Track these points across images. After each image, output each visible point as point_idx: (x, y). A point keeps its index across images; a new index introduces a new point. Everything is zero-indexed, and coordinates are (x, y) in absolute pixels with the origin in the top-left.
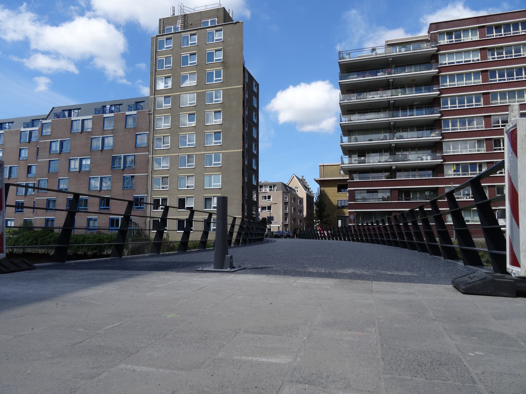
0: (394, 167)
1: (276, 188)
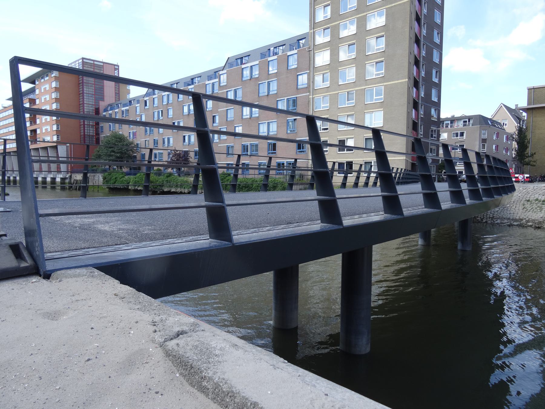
1: (471, 122)
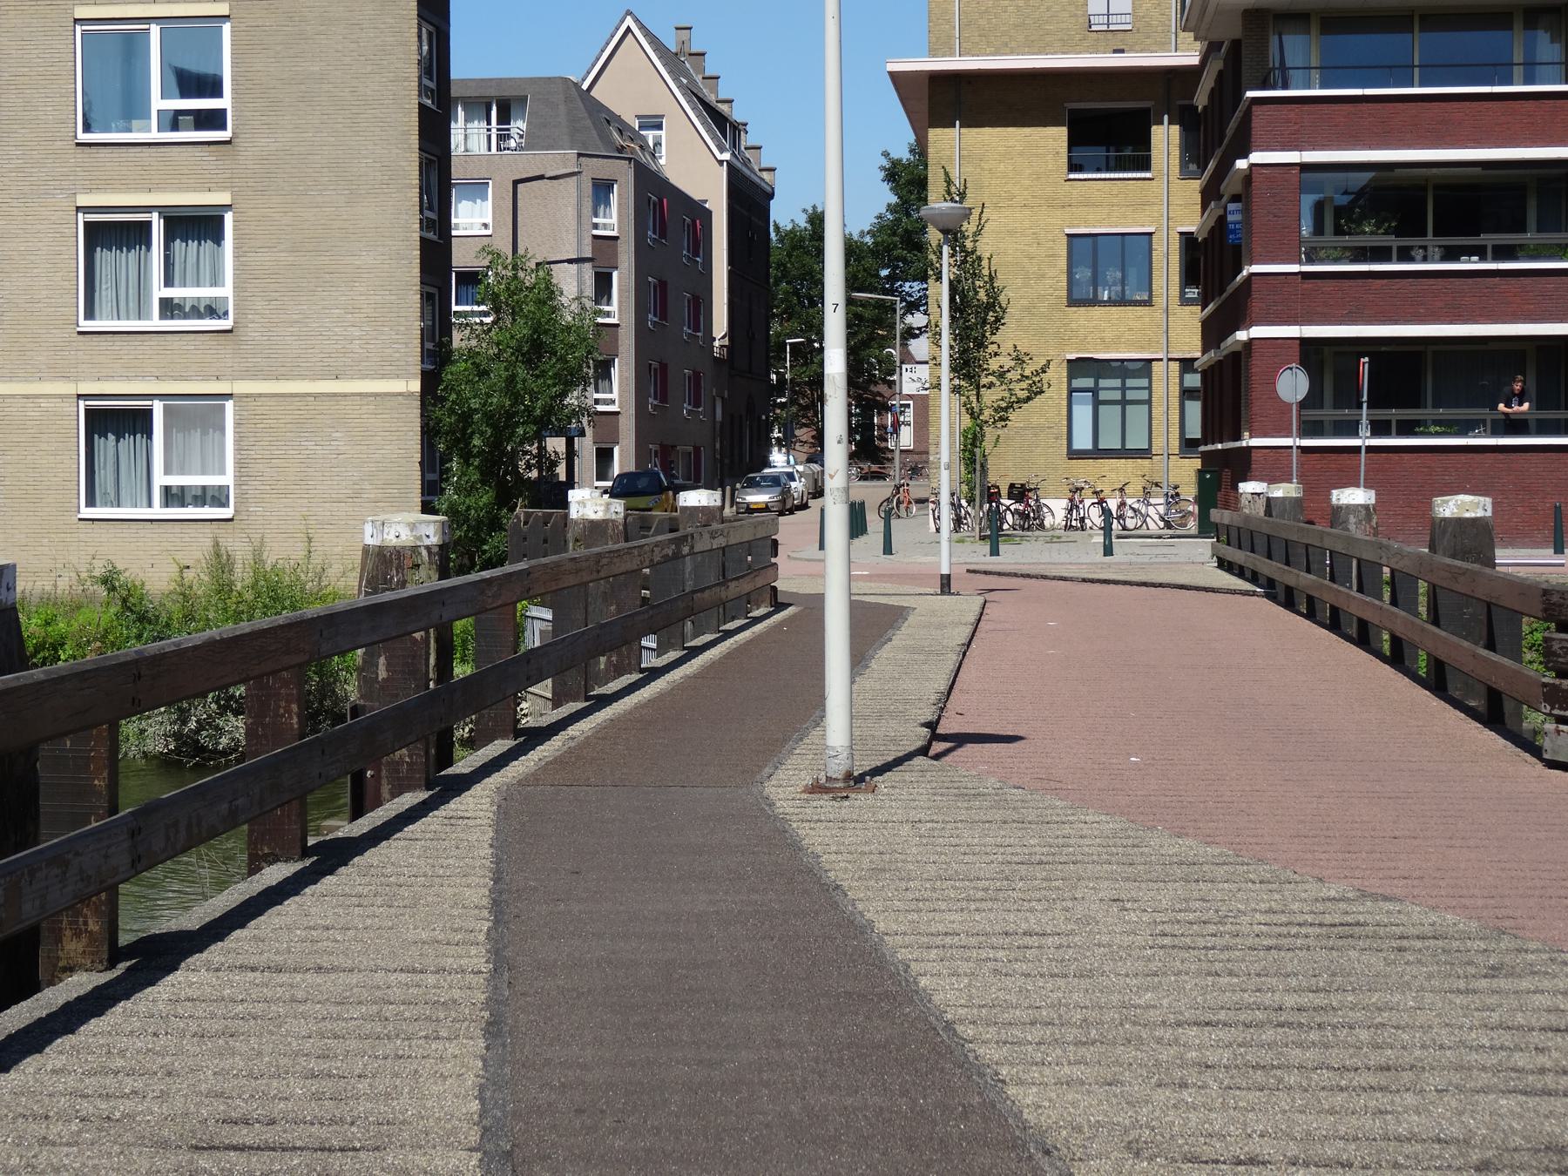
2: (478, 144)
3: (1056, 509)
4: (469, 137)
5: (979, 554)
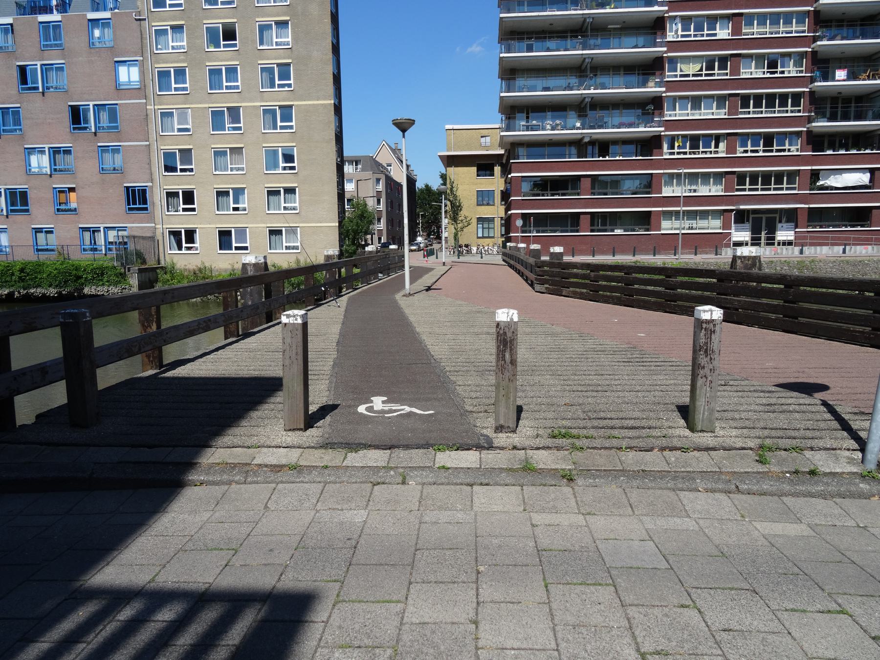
0: (586, 140)
2: (351, 171)
3: (474, 249)
4: (348, 169)
5: (455, 259)
